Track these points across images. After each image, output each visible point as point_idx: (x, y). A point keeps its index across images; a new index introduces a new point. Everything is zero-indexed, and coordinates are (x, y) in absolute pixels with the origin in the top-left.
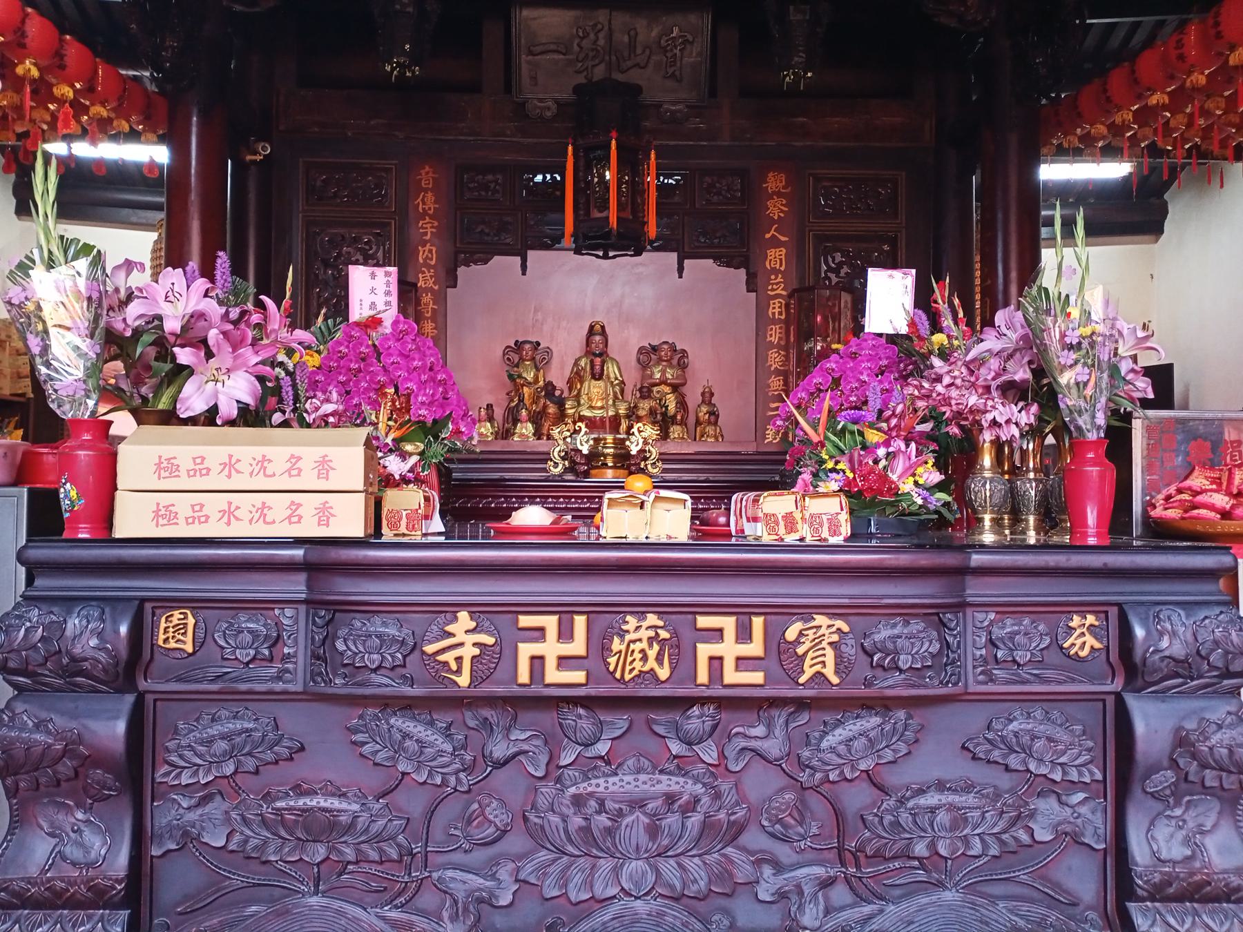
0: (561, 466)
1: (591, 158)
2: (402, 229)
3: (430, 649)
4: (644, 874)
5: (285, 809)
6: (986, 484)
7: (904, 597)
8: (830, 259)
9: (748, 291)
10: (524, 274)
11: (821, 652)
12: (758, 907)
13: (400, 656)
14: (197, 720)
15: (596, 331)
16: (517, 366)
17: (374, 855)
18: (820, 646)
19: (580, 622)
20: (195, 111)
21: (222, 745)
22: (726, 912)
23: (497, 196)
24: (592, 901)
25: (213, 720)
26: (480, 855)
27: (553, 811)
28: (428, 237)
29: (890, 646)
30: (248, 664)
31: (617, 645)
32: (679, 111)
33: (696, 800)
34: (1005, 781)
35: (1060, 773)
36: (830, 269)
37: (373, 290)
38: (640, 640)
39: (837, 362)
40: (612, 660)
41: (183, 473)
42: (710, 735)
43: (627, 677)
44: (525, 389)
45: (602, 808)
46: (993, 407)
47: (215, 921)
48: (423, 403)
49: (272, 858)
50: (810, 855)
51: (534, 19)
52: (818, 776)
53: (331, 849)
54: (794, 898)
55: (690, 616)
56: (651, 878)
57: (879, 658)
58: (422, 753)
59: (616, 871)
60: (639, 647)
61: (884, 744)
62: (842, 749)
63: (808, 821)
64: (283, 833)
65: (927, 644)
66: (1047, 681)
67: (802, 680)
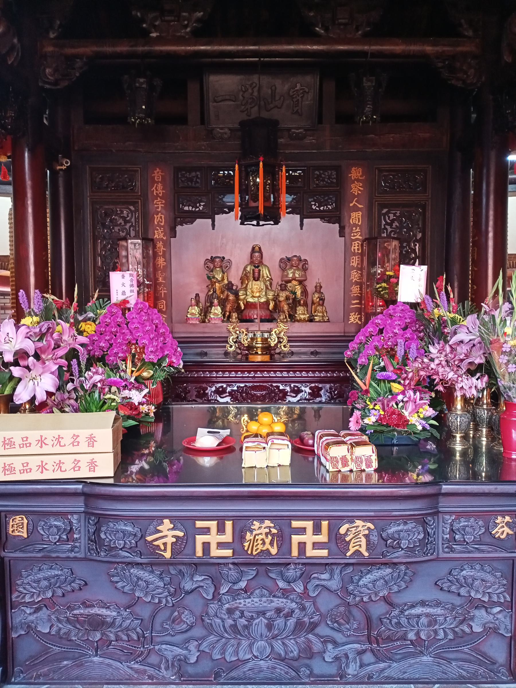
0: (234, 347)
1: (248, 171)
2: (145, 205)
3: (149, 538)
4: (265, 648)
5: (78, 615)
6: (458, 417)
7: (404, 510)
8: (387, 217)
9: (340, 237)
10: (213, 229)
11: (358, 540)
12: (325, 663)
13: (133, 541)
14: (32, 570)
15: (256, 250)
16: (212, 271)
17: (125, 638)
18: (358, 535)
19: (229, 524)
20: (27, 149)
21: (45, 583)
22: (308, 666)
23: (198, 185)
24: (238, 661)
25: (40, 570)
26: (179, 638)
27: (217, 616)
28: (159, 210)
29: (396, 536)
30: (55, 543)
31: (249, 536)
32: (301, 133)
33: (293, 611)
34: (458, 601)
35: (487, 598)
36: (387, 223)
37: (123, 285)
38: (261, 534)
39: (381, 319)
40: (246, 544)
41: (17, 446)
42: (300, 577)
43: (255, 553)
44: (217, 284)
45: (242, 615)
46: (462, 381)
47: (46, 669)
48: (152, 352)
49: (74, 639)
50: (352, 639)
51: (217, 81)
52: (358, 599)
53: (103, 634)
54: (344, 660)
55: (288, 521)
56: (268, 650)
57: (391, 543)
58: (148, 587)
59: (251, 646)
60: (260, 536)
61: (393, 583)
62: (370, 585)
63: (352, 621)
64: (78, 626)
65: (417, 534)
66: (483, 551)
67: (348, 554)
